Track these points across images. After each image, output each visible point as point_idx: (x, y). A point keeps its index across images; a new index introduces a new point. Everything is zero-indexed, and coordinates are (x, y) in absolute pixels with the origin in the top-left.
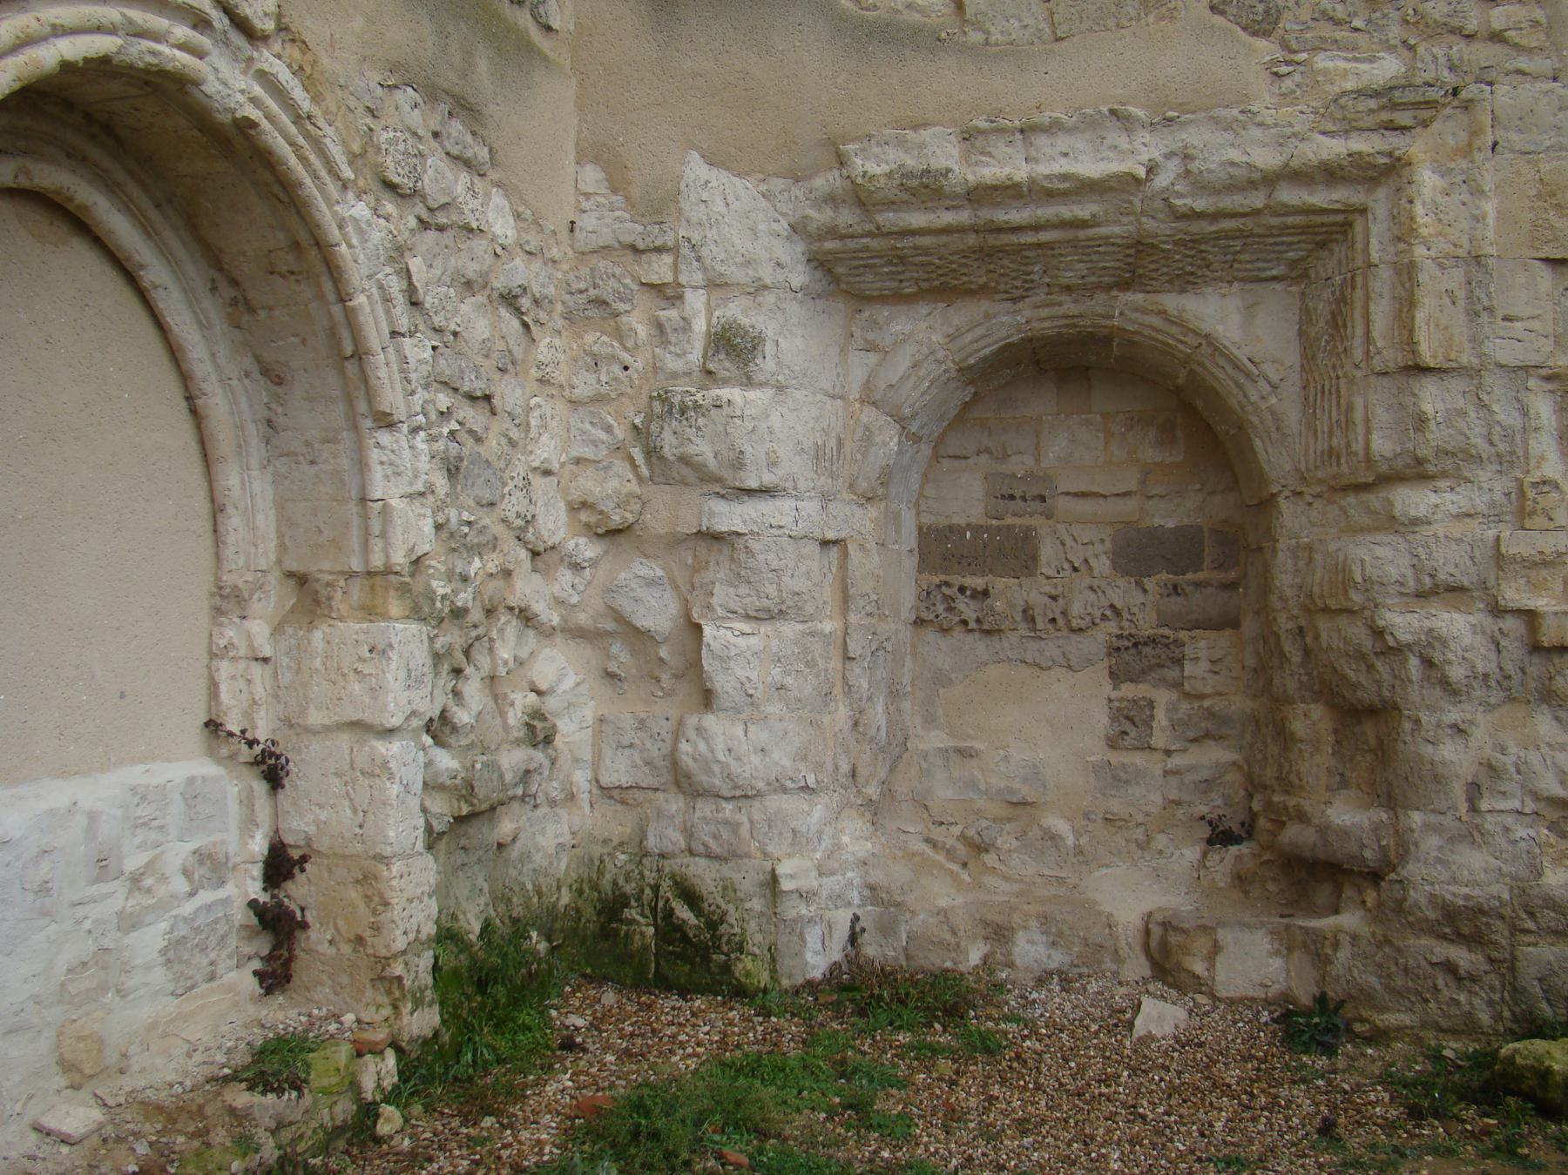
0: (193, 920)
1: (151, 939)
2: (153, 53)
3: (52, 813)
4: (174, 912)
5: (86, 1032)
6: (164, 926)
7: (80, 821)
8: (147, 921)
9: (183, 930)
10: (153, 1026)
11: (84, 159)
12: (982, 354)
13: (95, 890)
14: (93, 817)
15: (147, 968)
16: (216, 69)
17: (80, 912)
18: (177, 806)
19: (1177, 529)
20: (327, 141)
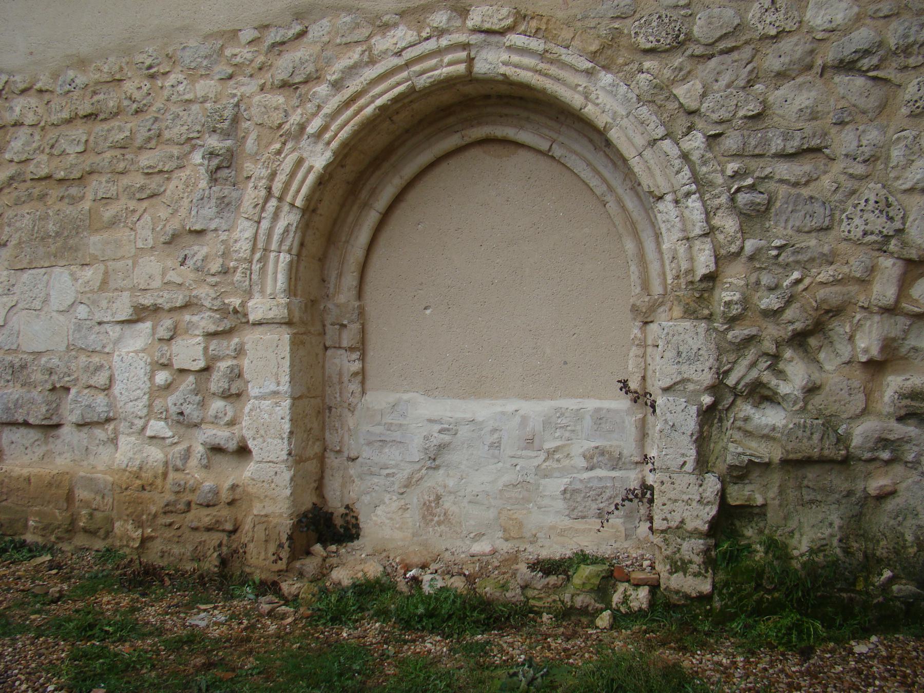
0: (588, 482)
1: (555, 485)
2: (429, 78)
3: (503, 413)
4: (574, 475)
5: (514, 517)
6: (566, 480)
7: (517, 419)
8: (555, 475)
9: (578, 486)
10: (552, 528)
11: (506, 115)
12: (379, 102)
13: (524, 453)
14: (524, 419)
15: (553, 498)
16: (48, 177)
17: (515, 461)
18: (588, 421)
19: (897, 630)
20: (563, 57)
